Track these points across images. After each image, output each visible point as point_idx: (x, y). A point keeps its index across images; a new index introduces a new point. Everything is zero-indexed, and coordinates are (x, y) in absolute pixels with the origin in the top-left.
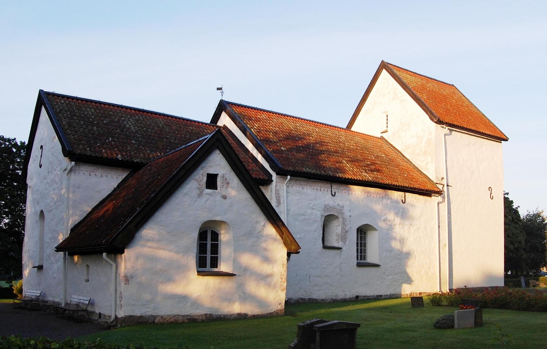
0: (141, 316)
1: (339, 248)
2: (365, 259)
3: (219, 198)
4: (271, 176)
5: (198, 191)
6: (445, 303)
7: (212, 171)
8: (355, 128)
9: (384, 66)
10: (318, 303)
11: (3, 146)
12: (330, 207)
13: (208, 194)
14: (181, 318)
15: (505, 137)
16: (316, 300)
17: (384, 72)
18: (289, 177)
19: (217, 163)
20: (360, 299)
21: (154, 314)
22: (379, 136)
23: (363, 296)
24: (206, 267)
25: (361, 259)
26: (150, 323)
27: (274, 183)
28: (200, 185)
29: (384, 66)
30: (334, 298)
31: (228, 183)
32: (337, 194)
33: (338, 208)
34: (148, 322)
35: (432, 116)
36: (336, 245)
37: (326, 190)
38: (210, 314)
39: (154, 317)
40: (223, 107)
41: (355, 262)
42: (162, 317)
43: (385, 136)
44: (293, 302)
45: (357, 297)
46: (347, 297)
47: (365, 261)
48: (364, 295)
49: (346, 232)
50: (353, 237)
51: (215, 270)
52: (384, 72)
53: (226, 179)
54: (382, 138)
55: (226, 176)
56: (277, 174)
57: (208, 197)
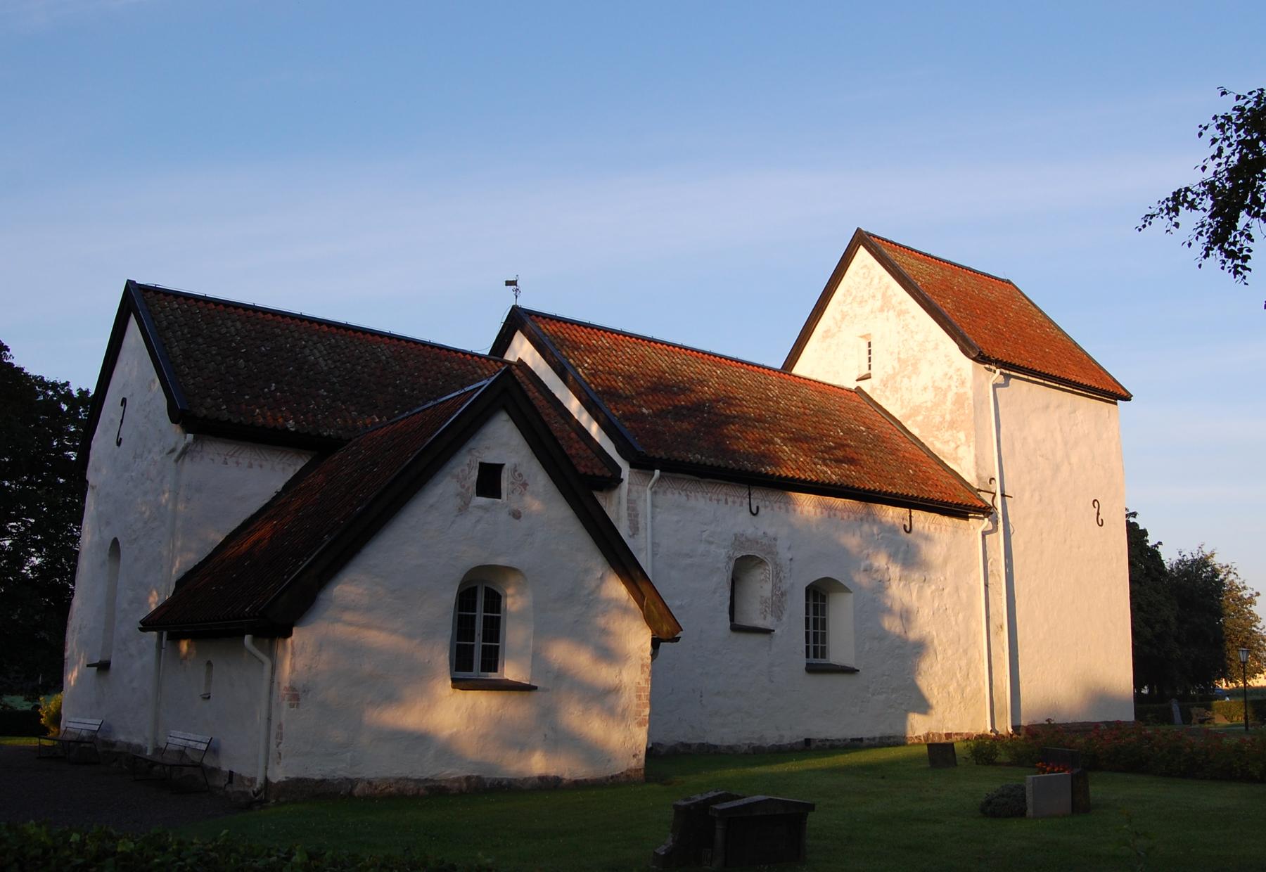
0: (323, 781)
1: (768, 632)
2: (823, 656)
3: (504, 516)
4: (620, 470)
7: (491, 458)
8: (797, 370)
9: (861, 239)
12: (748, 540)
14: (411, 785)
16: (716, 747)
18: (657, 472)
19: (502, 442)
20: (813, 746)
21: (351, 777)
23: (821, 741)
25: (815, 656)
27: (625, 485)
28: (463, 487)
30: (757, 743)
32: (762, 511)
33: (765, 541)
35: (966, 347)
36: (760, 623)
39: (353, 782)
40: (518, 320)
41: (802, 661)
42: (370, 783)
43: (865, 386)
46: (786, 741)
47: (823, 661)
48: (822, 736)
49: (783, 594)
50: (797, 605)
52: (862, 254)
53: (520, 475)
54: (859, 390)
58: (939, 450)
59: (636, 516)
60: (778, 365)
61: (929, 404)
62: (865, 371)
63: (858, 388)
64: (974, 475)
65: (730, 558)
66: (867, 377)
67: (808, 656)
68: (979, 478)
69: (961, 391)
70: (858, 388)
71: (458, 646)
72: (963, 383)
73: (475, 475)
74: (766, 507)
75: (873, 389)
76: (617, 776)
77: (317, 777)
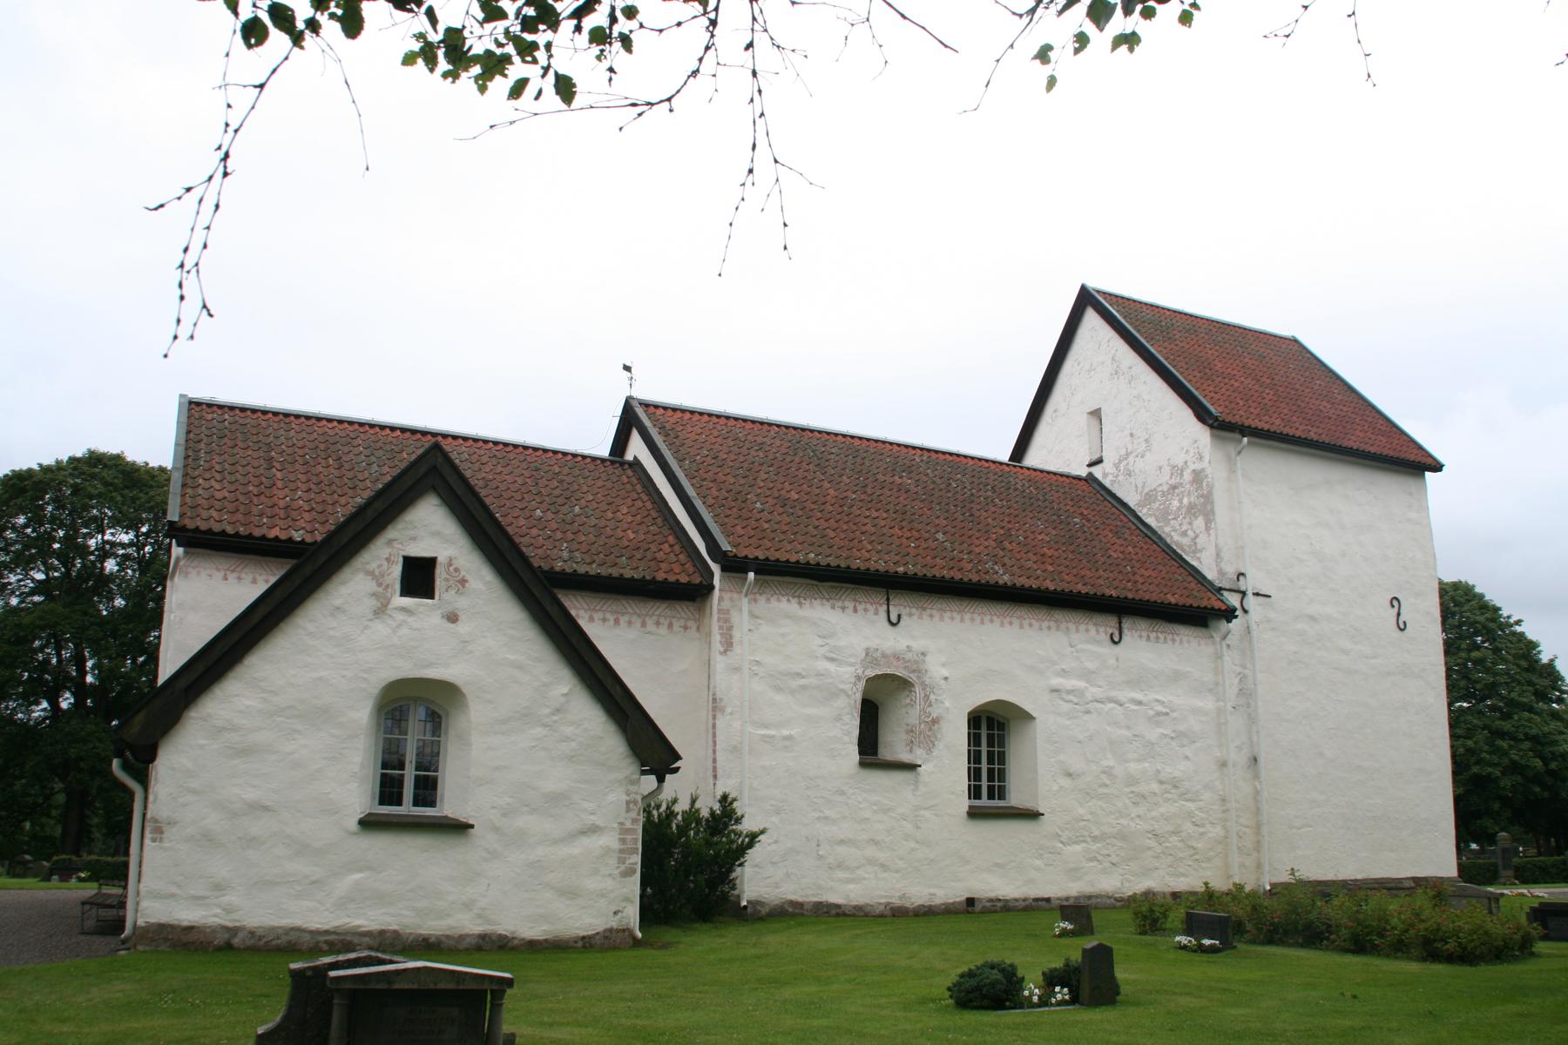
0: (191, 928)
1: (912, 767)
2: (1002, 797)
3: (436, 619)
4: (712, 574)
5: (374, 603)
6: (1177, 917)
7: (419, 550)
8: (1033, 459)
9: (1086, 299)
10: (845, 915)
11: (21, 520)
12: (884, 656)
13: (403, 609)
14: (307, 937)
15: (1429, 461)
16: (838, 906)
17: (1091, 318)
18: (751, 575)
19: (429, 529)
20: (978, 907)
21: (230, 924)
22: (1083, 472)
23: (991, 900)
24: (400, 804)
25: (991, 797)
26: (219, 949)
27: (716, 592)
28: (380, 585)
29: (1086, 299)
30: (896, 902)
31: (463, 582)
32: (904, 618)
33: (909, 656)
34: (210, 943)
35: (1202, 414)
36: (905, 757)
37: (871, 608)
38: (395, 931)
39: (234, 931)
40: (629, 420)
41: (964, 803)
42: (252, 933)
43: (1097, 471)
44: (764, 911)
45: (970, 901)
46: (937, 901)
47: (1001, 803)
48: (992, 895)
49: (935, 721)
50: (956, 735)
51: (428, 812)
52: (1091, 318)
53: (457, 570)
54: (1091, 479)
55: (457, 563)
56: (724, 569)
57: (400, 617)
58: (1177, 544)
59: (730, 628)
60: (1004, 455)
61: (1165, 488)
62: (1095, 457)
63: (1090, 474)
64: (1215, 570)
65: (858, 678)
66: (1099, 461)
67: (975, 792)
68: (1221, 573)
69: (1198, 466)
70: (1090, 474)
71: (383, 775)
72: (1201, 458)
73: (397, 570)
74: (911, 615)
75: (1105, 475)
76: (590, 937)
77: (185, 924)
